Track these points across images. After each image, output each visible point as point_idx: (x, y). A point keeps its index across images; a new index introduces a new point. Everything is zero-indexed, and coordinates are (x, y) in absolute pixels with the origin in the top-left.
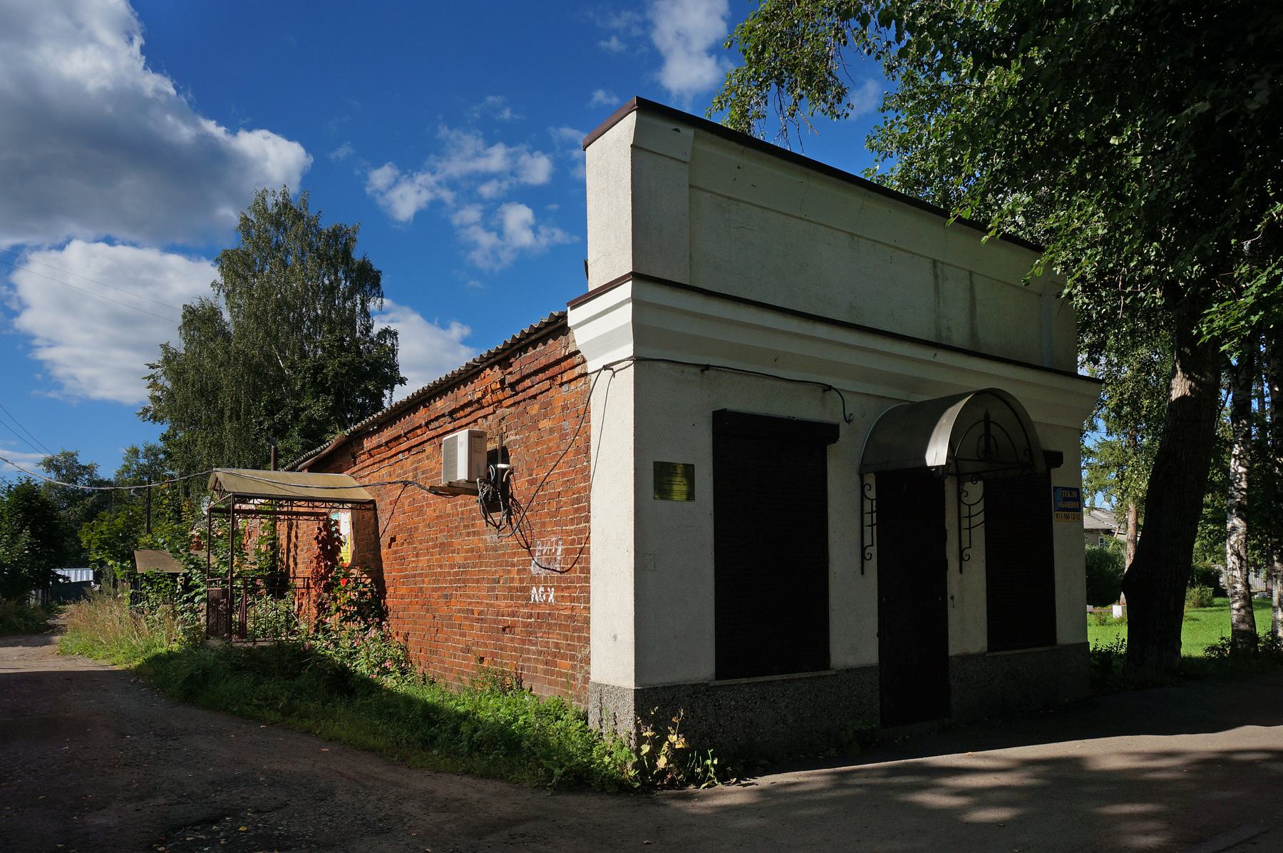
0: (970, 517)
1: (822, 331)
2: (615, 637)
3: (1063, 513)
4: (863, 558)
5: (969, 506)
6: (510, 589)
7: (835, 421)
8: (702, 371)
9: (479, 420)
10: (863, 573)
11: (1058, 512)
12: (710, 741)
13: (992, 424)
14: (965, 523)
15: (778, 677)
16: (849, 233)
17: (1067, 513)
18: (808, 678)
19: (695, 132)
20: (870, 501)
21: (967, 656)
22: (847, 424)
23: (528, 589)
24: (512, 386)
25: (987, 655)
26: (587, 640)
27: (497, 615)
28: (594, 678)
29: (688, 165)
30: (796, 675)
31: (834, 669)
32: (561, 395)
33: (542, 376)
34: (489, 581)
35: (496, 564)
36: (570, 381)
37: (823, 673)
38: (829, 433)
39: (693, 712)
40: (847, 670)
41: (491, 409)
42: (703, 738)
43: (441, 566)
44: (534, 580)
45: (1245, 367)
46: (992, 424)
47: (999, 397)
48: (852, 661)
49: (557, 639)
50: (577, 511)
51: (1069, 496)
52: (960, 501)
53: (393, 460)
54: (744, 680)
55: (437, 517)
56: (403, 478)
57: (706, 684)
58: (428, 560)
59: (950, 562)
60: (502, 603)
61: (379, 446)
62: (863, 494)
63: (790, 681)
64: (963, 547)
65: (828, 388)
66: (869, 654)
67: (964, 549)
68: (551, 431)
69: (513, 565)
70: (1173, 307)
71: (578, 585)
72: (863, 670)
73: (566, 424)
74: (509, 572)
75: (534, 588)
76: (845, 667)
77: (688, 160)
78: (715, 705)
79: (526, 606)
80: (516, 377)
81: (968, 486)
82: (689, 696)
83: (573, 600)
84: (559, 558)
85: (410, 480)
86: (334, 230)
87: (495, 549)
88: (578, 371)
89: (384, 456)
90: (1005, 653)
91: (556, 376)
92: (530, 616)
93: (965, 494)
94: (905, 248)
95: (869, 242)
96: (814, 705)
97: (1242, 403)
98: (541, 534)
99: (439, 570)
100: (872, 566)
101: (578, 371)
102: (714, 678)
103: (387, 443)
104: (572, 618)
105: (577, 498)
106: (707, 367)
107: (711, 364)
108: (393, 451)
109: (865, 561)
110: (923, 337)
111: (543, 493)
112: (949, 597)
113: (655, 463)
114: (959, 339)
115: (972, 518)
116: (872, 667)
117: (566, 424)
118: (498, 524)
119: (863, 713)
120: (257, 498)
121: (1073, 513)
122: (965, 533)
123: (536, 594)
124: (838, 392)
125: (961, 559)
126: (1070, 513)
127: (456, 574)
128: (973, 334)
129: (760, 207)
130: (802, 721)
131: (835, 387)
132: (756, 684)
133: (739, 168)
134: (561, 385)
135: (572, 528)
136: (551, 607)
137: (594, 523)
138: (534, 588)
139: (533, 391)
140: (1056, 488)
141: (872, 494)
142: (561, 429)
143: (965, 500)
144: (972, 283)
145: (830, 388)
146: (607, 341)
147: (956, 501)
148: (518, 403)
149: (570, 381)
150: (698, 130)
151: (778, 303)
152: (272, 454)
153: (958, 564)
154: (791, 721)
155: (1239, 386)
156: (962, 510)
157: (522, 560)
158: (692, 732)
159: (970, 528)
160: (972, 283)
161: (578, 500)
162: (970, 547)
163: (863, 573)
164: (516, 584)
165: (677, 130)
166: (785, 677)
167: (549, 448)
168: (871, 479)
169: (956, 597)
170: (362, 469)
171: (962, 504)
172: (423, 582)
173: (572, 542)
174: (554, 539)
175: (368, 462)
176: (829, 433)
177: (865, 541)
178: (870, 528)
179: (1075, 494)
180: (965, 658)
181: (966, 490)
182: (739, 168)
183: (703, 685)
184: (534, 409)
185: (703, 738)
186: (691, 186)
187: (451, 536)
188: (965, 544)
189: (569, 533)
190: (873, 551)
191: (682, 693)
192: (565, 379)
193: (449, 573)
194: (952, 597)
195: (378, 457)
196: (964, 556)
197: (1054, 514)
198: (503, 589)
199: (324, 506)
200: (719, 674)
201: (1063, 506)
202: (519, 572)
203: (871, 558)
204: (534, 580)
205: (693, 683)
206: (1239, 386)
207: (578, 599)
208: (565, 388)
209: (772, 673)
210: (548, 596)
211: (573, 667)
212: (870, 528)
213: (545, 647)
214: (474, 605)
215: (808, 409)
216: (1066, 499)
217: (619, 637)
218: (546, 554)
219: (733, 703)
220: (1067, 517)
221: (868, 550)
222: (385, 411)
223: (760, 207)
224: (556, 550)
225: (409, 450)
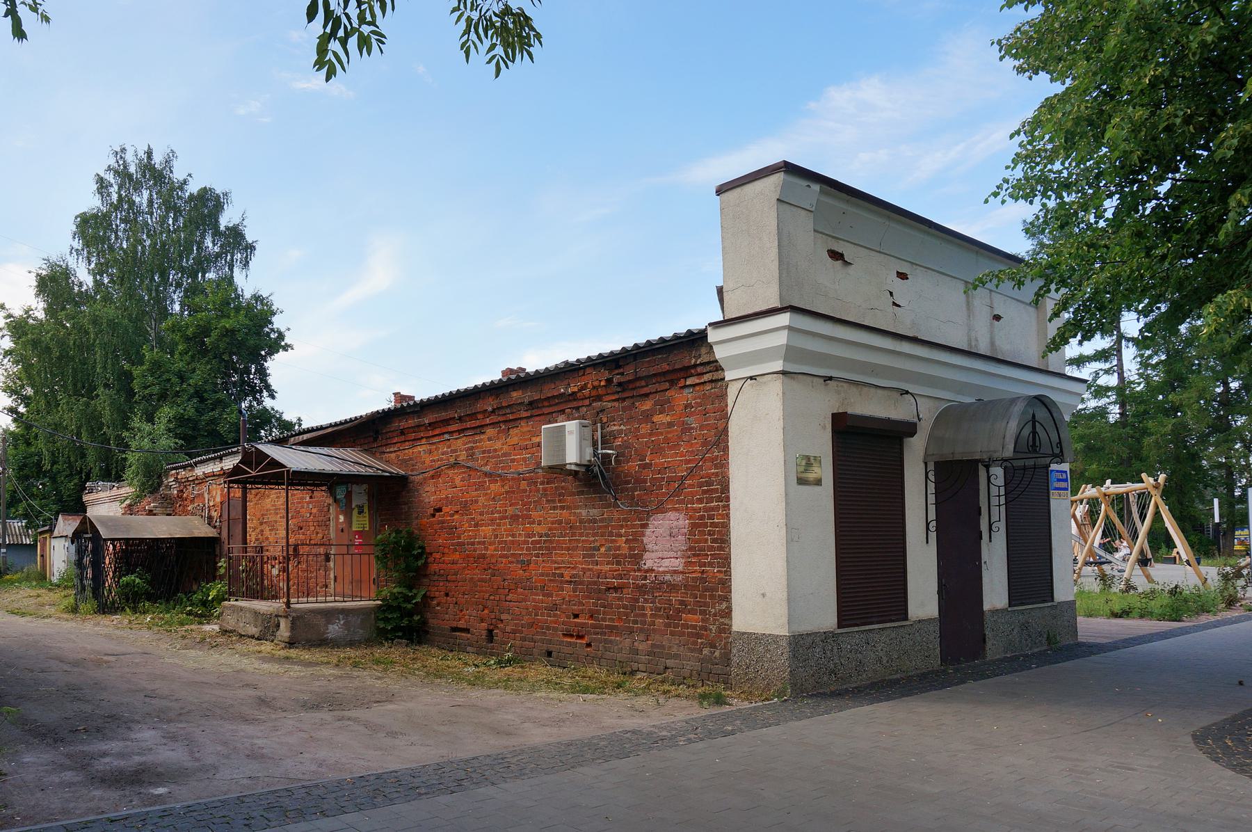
1: (906, 347)
3: (1057, 491)
8: (825, 381)
10: (927, 542)
15: (876, 626)
16: (963, 280)
18: (894, 627)
28: (735, 628)
30: (888, 625)
38: (909, 429)
41: (587, 402)
51: (1061, 478)
54: (856, 629)
55: (507, 492)
58: (494, 530)
62: (927, 477)
63: (883, 629)
71: (709, 553)
76: (917, 617)
77: (813, 209)
82: (823, 641)
86: (1095, 398)
94: (953, 275)
95: (923, 269)
100: (933, 536)
102: (836, 626)
106: (831, 378)
111: (659, 476)
114: (983, 349)
129: (910, 262)
132: (862, 632)
145: (907, 392)
147: (986, 481)
150: (822, 185)
152: (1168, 525)
156: (991, 490)
157: (633, 531)
163: (927, 542)
165: (808, 186)
166: (881, 626)
171: (991, 486)
176: (909, 429)
180: (995, 612)
186: (815, 231)
193: (526, 542)
194: (985, 562)
198: (605, 555)
200: (840, 625)
202: (627, 541)
208: (687, 391)
213: (667, 604)
214: (563, 569)
225: (459, 431)
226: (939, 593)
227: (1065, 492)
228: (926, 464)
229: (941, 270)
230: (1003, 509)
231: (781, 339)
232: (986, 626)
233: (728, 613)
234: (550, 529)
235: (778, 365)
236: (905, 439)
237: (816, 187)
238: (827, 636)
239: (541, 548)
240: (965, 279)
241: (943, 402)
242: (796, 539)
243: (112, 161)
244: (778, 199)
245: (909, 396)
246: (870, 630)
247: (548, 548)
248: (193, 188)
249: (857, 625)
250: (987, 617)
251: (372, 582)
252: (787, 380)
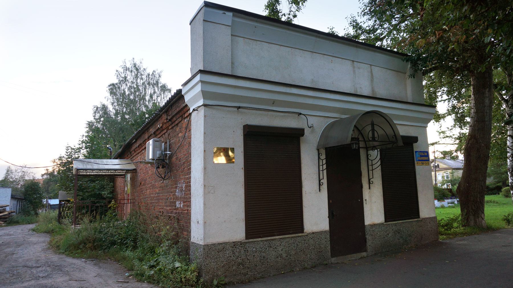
0: (372, 165)
3: (420, 162)
4: (320, 185)
5: (372, 160)
6: (171, 202)
8: (238, 109)
11: (418, 162)
12: (243, 266)
13: (375, 125)
15: (277, 237)
16: (351, 60)
17: (423, 162)
19: (233, 14)
20: (371, 161)
21: (374, 225)
22: (309, 128)
24: (170, 120)
25: (385, 224)
29: (230, 27)
31: (306, 232)
33: (178, 116)
37: (300, 235)
39: (234, 254)
40: (313, 233)
42: (239, 265)
44: (177, 198)
45: (511, 99)
46: (375, 125)
47: (382, 116)
49: (183, 223)
51: (423, 155)
54: (260, 239)
57: (240, 242)
59: (364, 185)
61: (136, 148)
62: (319, 158)
63: (283, 239)
64: (370, 178)
67: (321, 180)
70: (413, 61)
72: (321, 233)
76: (312, 231)
77: (230, 25)
78: (245, 251)
80: (171, 117)
81: (371, 152)
84: (184, 189)
89: (138, 151)
90: (394, 222)
91: (183, 115)
93: (370, 155)
96: (296, 249)
97: (510, 114)
100: (325, 187)
103: (138, 146)
106: (239, 108)
107: (240, 106)
108: (141, 150)
109: (371, 184)
112: (364, 200)
115: (373, 166)
116: (325, 231)
118: (163, 177)
119: (321, 251)
120: (94, 170)
121: (425, 162)
122: (371, 172)
124: (304, 115)
125: (369, 183)
126: (424, 162)
127: (157, 197)
128: (373, 91)
129: (311, 52)
130: (290, 256)
131: (303, 113)
133: (255, 27)
135: (187, 176)
137: (192, 175)
139: (177, 122)
140: (416, 152)
141: (323, 157)
143: (370, 158)
144: (371, 70)
145: (301, 114)
146: (194, 99)
150: (233, 13)
153: (368, 185)
154: (284, 256)
155: (509, 107)
158: (234, 263)
159: (372, 170)
160: (371, 70)
162: (373, 178)
163: (320, 191)
166: (281, 237)
168: (323, 152)
169: (367, 200)
170: (134, 157)
175: (135, 154)
177: (320, 177)
178: (322, 171)
179: (426, 154)
180: (373, 226)
181: (320, 153)
182: (255, 27)
183: (239, 242)
185: (239, 265)
186: (232, 35)
188: (371, 177)
191: (228, 246)
194: (366, 200)
195: (137, 152)
196: (321, 183)
197: (416, 162)
199: (122, 172)
200: (247, 237)
201: (420, 159)
203: (373, 183)
205: (234, 241)
206: (509, 107)
212: (322, 171)
216: (421, 156)
217: (199, 222)
219: (254, 249)
220: (423, 164)
222: (135, 134)
223: (311, 52)
226: (329, 217)
227: (428, 162)
228: (318, 150)
229: (333, 55)
230: (325, 172)
231: (198, 88)
232: (366, 233)
235: (201, 102)
236: (300, 138)
237: (231, 14)
240: (352, 60)
241: (331, 119)
242: (212, 191)
243: (122, 64)
244: (204, 20)
245: (302, 116)
246: (272, 240)
247: (157, 199)
248: (150, 71)
249: (261, 237)
250: (367, 230)
251: (125, 214)
252: (207, 109)
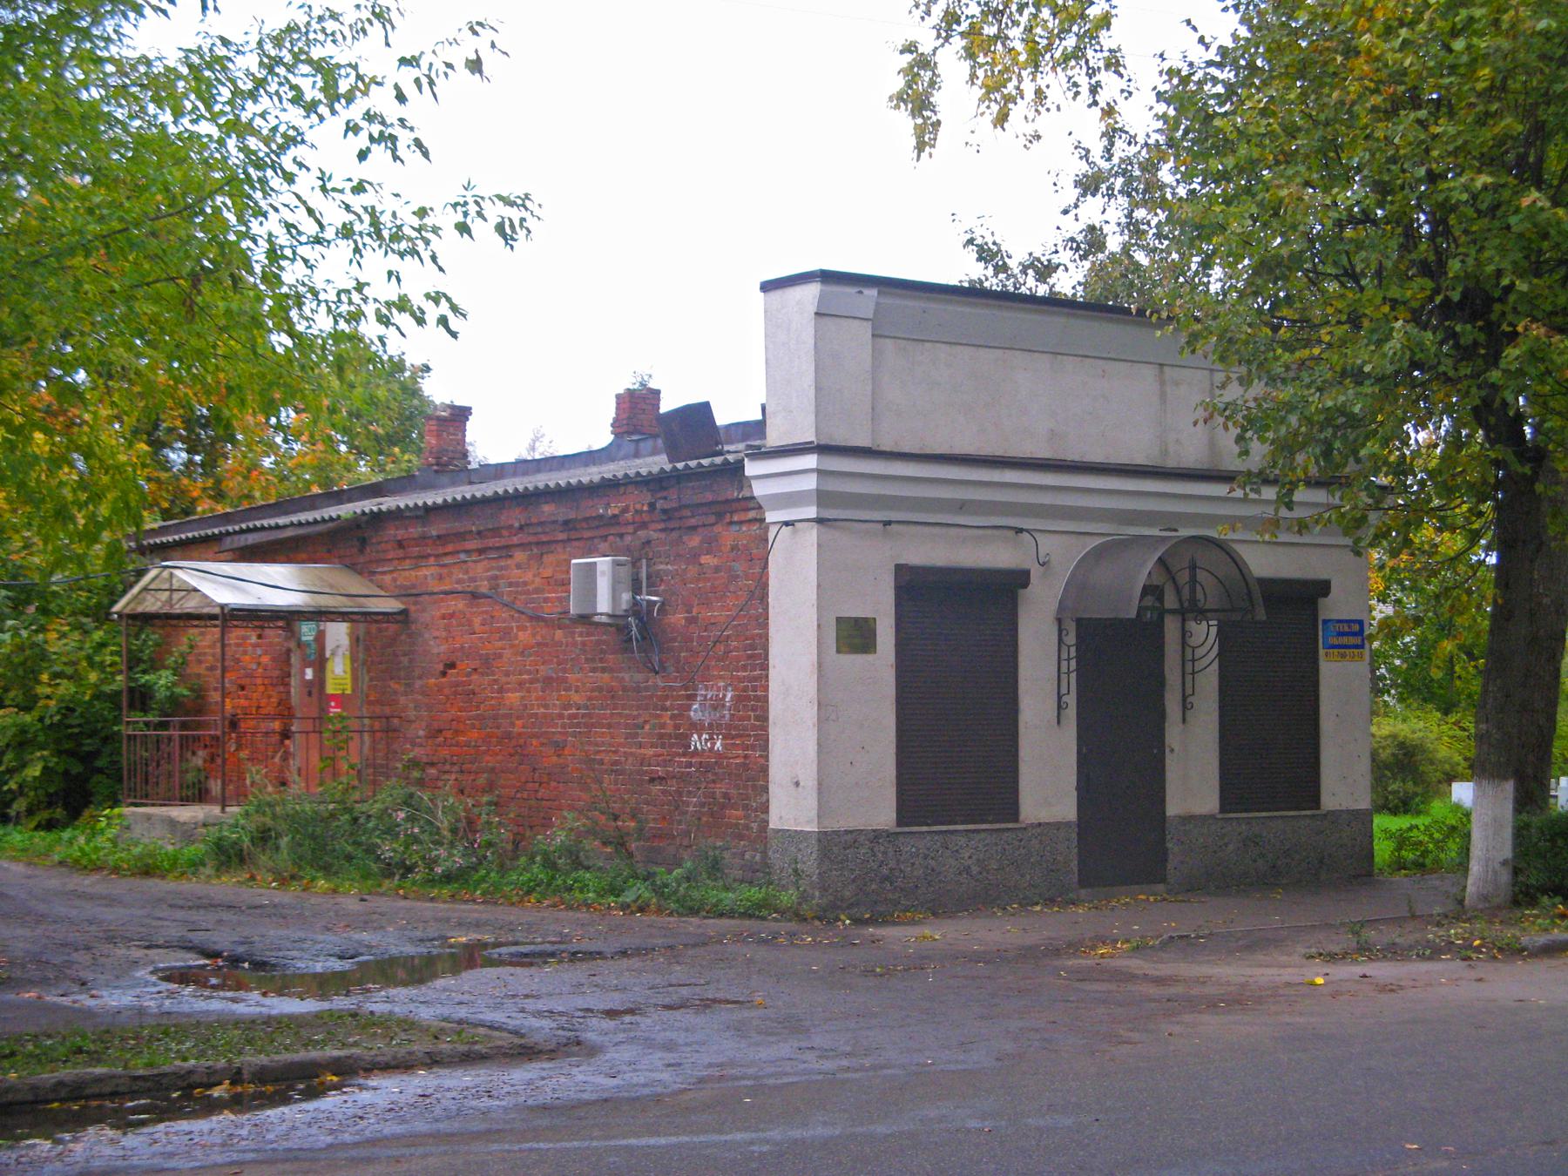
2: (797, 784)
3: (1336, 651)
6: (661, 736)
7: (1025, 566)
9: (611, 538)
14: (1189, 668)
23: (688, 737)
26: (766, 789)
27: (641, 765)
32: (729, 536)
34: (627, 726)
35: (638, 708)
36: (741, 523)
37: (1010, 825)
41: (630, 529)
43: (546, 707)
44: (697, 727)
48: (1044, 815)
50: (750, 657)
51: (1346, 629)
52: (1184, 643)
53: (448, 560)
55: (538, 644)
56: (472, 587)
60: (651, 752)
62: (1060, 641)
63: (974, 831)
65: (1019, 531)
66: (1066, 809)
68: (717, 569)
69: (664, 709)
72: (1058, 826)
73: (736, 565)
74: (659, 716)
75: (695, 736)
79: (684, 755)
81: (1192, 625)
83: (746, 748)
85: (484, 590)
87: (637, 689)
88: (752, 514)
92: (690, 765)
98: (705, 679)
99: (542, 710)
100: (1071, 712)
101: (752, 514)
104: (745, 767)
105: (750, 645)
106: (887, 523)
110: (1140, 459)
113: (839, 620)
117: (736, 565)
122: (1189, 678)
123: (697, 743)
126: (1347, 651)
134: (731, 523)
136: (719, 755)
138: (695, 736)
140: (1325, 622)
142: (730, 569)
148: (672, 530)
149: (741, 523)
151: (1096, 456)
161: (752, 647)
163: (1059, 722)
164: (669, 730)
165: (860, 292)
167: (713, 587)
168: (1071, 628)
172: (513, 725)
173: (745, 689)
174: (721, 684)
176: (1020, 579)
179: (1356, 628)
183: (883, 831)
184: (694, 541)
187: (565, 671)
188: (1188, 691)
189: (741, 680)
190: (1071, 700)
192: (736, 518)
197: (1322, 652)
204: (697, 727)
207: (753, 747)
209: (956, 823)
210: (713, 744)
211: (747, 817)
215: (997, 556)
218: (711, 699)
221: (1064, 699)
224: (724, 696)
225: (481, 551)
233: (765, 808)
234: (590, 699)
238: (877, 835)
239: (578, 725)
